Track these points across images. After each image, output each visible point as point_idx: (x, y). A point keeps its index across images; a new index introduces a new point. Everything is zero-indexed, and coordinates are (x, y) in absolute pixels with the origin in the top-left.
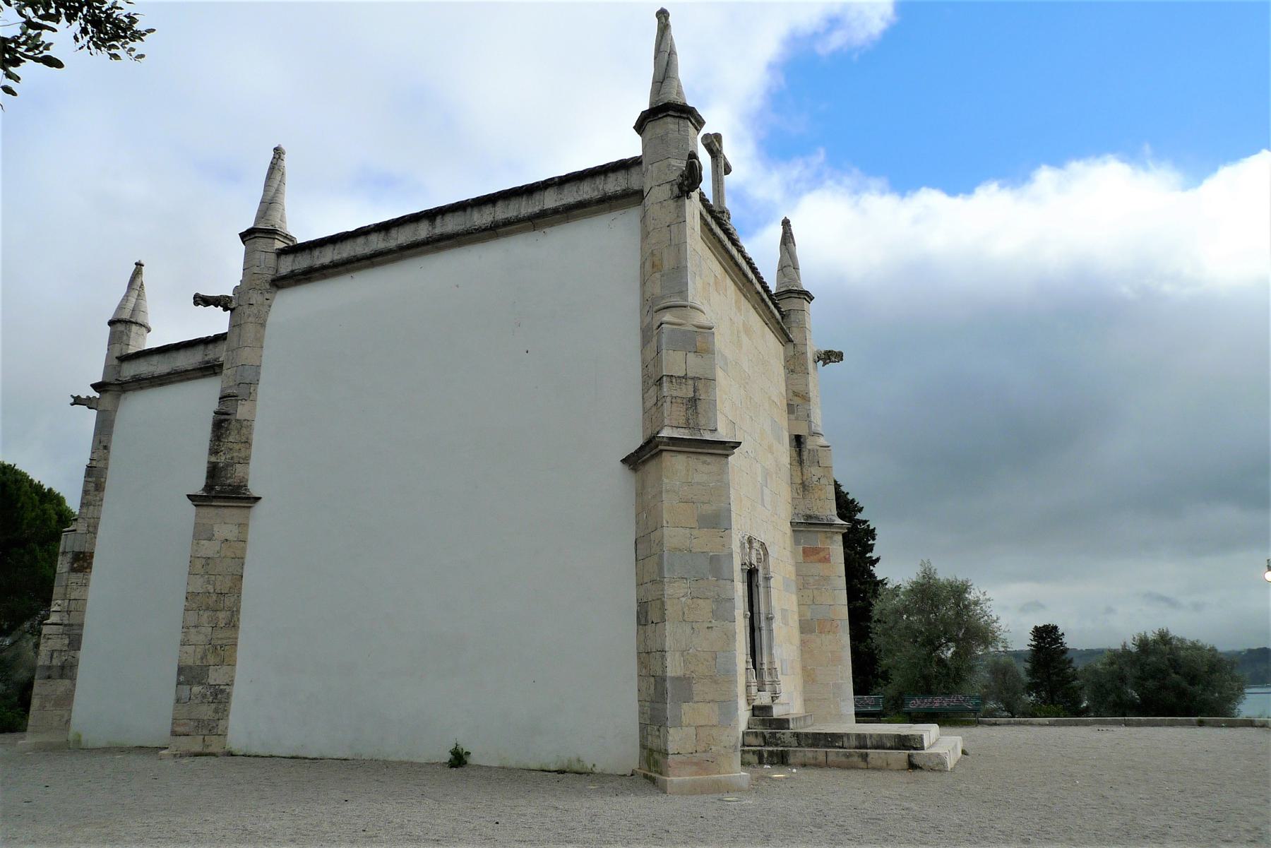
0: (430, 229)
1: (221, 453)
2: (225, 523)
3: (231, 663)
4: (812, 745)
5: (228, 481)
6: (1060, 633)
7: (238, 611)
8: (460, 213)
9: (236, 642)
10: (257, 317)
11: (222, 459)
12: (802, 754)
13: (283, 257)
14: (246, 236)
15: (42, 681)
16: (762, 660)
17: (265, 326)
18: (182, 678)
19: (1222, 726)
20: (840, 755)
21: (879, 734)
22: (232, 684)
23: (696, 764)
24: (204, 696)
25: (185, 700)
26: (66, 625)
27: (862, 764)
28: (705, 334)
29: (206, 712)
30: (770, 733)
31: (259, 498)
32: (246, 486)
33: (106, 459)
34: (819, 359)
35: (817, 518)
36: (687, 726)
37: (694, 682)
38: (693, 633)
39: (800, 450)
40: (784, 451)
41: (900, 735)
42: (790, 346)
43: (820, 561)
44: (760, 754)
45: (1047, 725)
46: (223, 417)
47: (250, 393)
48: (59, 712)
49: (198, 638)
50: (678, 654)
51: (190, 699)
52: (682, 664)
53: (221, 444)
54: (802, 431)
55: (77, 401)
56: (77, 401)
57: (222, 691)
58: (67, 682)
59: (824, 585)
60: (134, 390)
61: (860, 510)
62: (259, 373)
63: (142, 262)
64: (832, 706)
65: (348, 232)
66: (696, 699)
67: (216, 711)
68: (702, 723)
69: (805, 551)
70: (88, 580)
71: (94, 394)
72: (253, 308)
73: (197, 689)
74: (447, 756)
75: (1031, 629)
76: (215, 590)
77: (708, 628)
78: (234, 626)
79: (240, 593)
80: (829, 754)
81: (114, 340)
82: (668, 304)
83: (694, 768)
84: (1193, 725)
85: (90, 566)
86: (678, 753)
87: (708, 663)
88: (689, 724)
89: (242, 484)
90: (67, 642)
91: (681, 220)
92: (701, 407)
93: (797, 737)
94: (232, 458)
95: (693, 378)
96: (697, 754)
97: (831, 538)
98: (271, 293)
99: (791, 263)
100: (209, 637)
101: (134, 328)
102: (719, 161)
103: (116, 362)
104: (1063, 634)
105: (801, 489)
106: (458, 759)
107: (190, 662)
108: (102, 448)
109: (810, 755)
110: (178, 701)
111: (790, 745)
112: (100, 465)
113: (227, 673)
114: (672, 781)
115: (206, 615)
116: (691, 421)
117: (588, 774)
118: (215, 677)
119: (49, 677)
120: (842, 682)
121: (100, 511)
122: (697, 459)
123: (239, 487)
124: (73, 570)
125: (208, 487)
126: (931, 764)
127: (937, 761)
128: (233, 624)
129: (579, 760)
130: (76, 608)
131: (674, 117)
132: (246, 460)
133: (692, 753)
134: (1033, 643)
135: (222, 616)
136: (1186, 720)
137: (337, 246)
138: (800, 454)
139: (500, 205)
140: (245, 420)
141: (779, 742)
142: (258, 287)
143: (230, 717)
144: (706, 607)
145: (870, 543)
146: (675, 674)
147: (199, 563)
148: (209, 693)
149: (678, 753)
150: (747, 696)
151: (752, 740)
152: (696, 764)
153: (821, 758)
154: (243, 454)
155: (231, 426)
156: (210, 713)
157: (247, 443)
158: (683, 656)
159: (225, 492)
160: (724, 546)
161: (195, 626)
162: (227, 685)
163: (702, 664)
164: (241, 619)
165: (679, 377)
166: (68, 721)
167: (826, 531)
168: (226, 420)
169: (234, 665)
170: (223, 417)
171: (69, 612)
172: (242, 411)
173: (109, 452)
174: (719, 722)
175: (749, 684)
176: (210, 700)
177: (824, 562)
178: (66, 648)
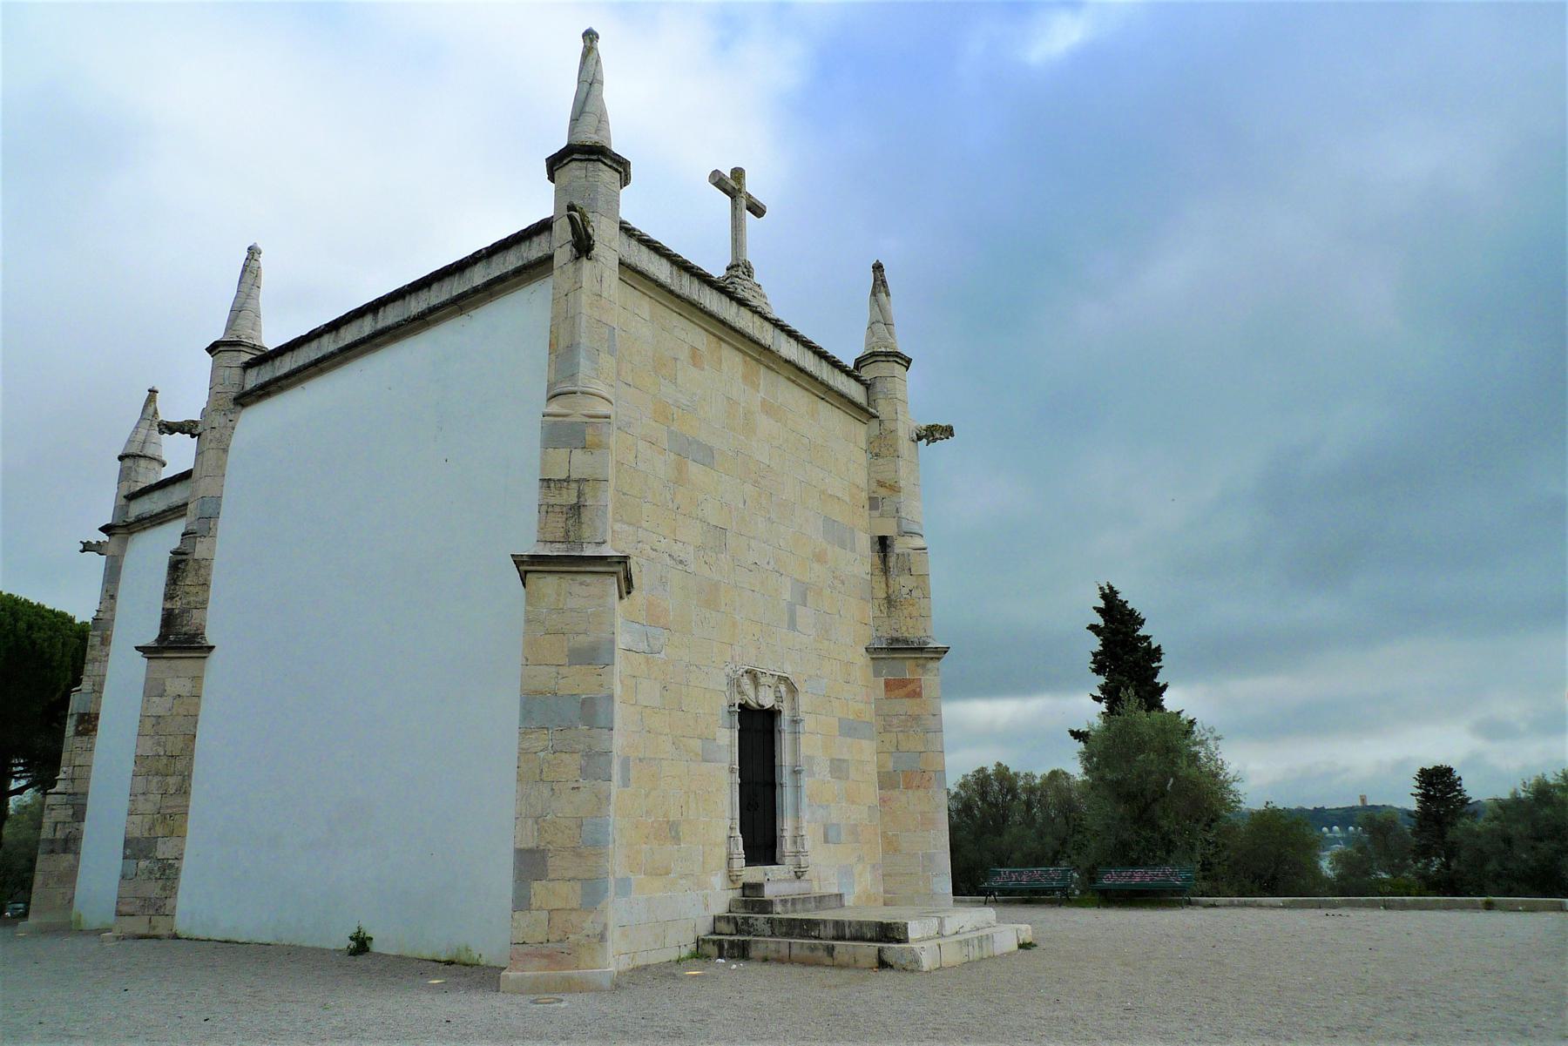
0: (373, 324)
1: (177, 599)
2: (178, 677)
3: (180, 834)
4: (787, 935)
5: (184, 629)
6: (1456, 777)
7: (190, 776)
8: (399, 303)
9: (187, 810)
10: (219, 441)
11: (177, 605)
12: (764, 946)
13: (249, 371)
14: (213, 349)
15: (45, 856)
16: (783, 826)
17: (227, 451)
18: (128, 852)
19: (1520, 911)
20: (805, 947)
21: (859, 922)
22: (182, 858)
23: (548, 956)
24: (151, 872)
25: (131, 877)
26: (70, 794)
27: (828, 961)
28: (599, 425)
29: (154, 889)
30: (743, 918)
31: (213, 647)
32: (202, 634)
33: (113, 610)
34: (920, 438)
35: (906, 641)
36: (537, 910)
37: (550, 855)
38: (553, 795)
39: (885, 556)
40: (859, 561)
41: (882, 923)
42: (875, 423)
43: (908, 696)
44: (720, 944)
45: (1281, 907)
46: (180, 557)
47: (210, 529)
48: (62, 890)
49: (146, 806)
50: (530, 822)
51: (136, 875)
52: (536, 834)
53: (177, 587)
54: (888, 529)
55: (87, 547)
56: (87, 547)
57: (171, 866)
58: (70, 857)
59: (912, 727)
60: (138, 531)
61: (1142, 622)
62: (220, 505)
63: (156, 389)
64: (921, 883)
65: (302, 336)
66: (551, 876)
67: (164, 888)
68: (559, 904)
69: (887, 684)
70: (93, 744)
71: (104, 537)
72: (215, 431)
73: (143, 864)
74: (345, 943)
75: (1416, 771)
76: (166, 752)
77: (573, 788)
78: (185, 793)
79: (193, 755)
80: (793, 947)
81: (124, 476)
82: (565, 390)
83: (545, 962)
84: (1478, 908)
85: (95, 728)
86: (524, 943)
87: (571, 832)
88: (541, 907)
89: (199, 632)
90: (70, 812)
91: (578, 285)
92: (586, 515)
93: (771, 923)
94: (189, 603)
95: (577, 481)
96: (549, 945)
97: (924, 666)
98: (235, 413)
99: (881, 318)
100: (158, 806)
101: (143, 462)
102: (738, 202)
103: (124, 501)
104: (1460, 778)
105: (886, 605)
106: (361, 945)
107: (137, 834)
108: (108, 597)
109: (772, 947)
110: (123, 877)
111: (762, 933)
112: (107, 616)
113: (176, 846)
114: (507, 977)
115: (156, 779)
116: (571, 534)
117: (472, 965)
118: (164, 850)
119: (52, 851)
120: (935, 851)
121: (105, 667)
122: (572, 580)
123: (196, 635)
124: (78, 733)
125: (162, 637)
126: (903, 962)
127: (910, 957)
128: (184, 791)
129: (467, 950)
130: (82, 775)
131: (581, 160)
132: (203, 605)
133: (542, 943)
134: (1421, 791)
135: (172, 781)
136: (1466, 901)
137: (295, 353)
138: (884, 560)
139: (686, 278)
140: (203, 559)
141: (752, 930)
142: (220, 408)
143: (179, 893)
144: (572, 763)
145: (1154, 665)
146: (525, 846)
147: (149, 723)
148: (156, 868)
149: (524, 943)
150: (730, 871)
151: (723, 926)
152: (548, 956)
153: (785, 951)
154: (200, 599)
155: (188, 568)
156: (158, 890)
157: (205, 585)
158: (537, 823)
159: (182, 642)
160: (601, 685)
161: (144, 793)
162: (176, 859)
163: (563, 832)
164: (192, 785)
165: (559, 480)
166: (71, 901)
167: (917, 658)
168: (184, 561)
169: (184, 837)
170: (180, 557)
171: (73, 780)
172: (200, 550)
173: (116, 602)
174: (580, 904)
175: (731, 857)
176: (158, 876)
177: (914, 697)
178: (70, 819)
